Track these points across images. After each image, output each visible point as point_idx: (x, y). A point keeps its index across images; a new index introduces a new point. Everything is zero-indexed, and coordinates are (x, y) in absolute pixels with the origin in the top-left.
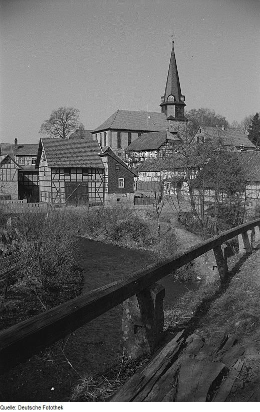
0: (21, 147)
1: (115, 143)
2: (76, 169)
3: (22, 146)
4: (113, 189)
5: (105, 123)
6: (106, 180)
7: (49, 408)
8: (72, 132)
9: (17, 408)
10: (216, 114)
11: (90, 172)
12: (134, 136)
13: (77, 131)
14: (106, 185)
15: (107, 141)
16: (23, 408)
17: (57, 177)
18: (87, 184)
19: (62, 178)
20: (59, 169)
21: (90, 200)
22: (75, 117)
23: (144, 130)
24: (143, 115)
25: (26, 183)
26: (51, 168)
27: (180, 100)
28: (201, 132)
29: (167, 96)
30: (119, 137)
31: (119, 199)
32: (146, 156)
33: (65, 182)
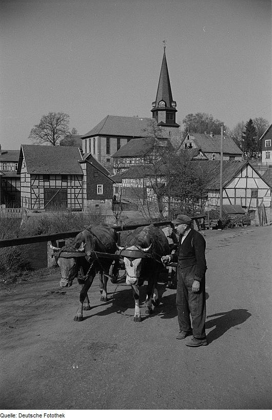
0: (5, 153)
1: (104, 148)
2: (56, 176)
3: (6, 153)
4: (92, 195)
5: (95, 129)
6: (85, 186)
7: (50, 416)
8: (62, 137)
9: (17, 416)
10: (214, 119)
11: (69, 178)
12: (124, 142)
13: (67, 136)
14: (85, 191)
15: (95, 149)
16: (23, 416)
17: (36, 183)
18: (67, 191)
19: (42, 184)
20: (39, 175)
21: (69, 206)
22: (65, 122)
23: (133, 135)
24: (135, 119)
25: (9, 189)
26: (31, 174)
27: (171, 106)
28: (188, 139)
29: (158, 102)
30: (108, 142)
31: (97, 206)
32: (133, 162)
33: (44, 189)
